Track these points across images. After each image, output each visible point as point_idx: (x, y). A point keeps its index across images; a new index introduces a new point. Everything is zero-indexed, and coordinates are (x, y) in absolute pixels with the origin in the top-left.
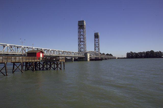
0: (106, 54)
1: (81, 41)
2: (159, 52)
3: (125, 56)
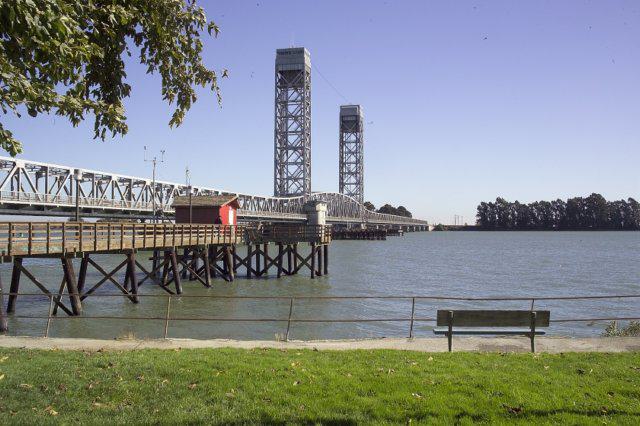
0: (378, 207)
1: (290, 143)
2: (627, 201)
3: (473, 221)
